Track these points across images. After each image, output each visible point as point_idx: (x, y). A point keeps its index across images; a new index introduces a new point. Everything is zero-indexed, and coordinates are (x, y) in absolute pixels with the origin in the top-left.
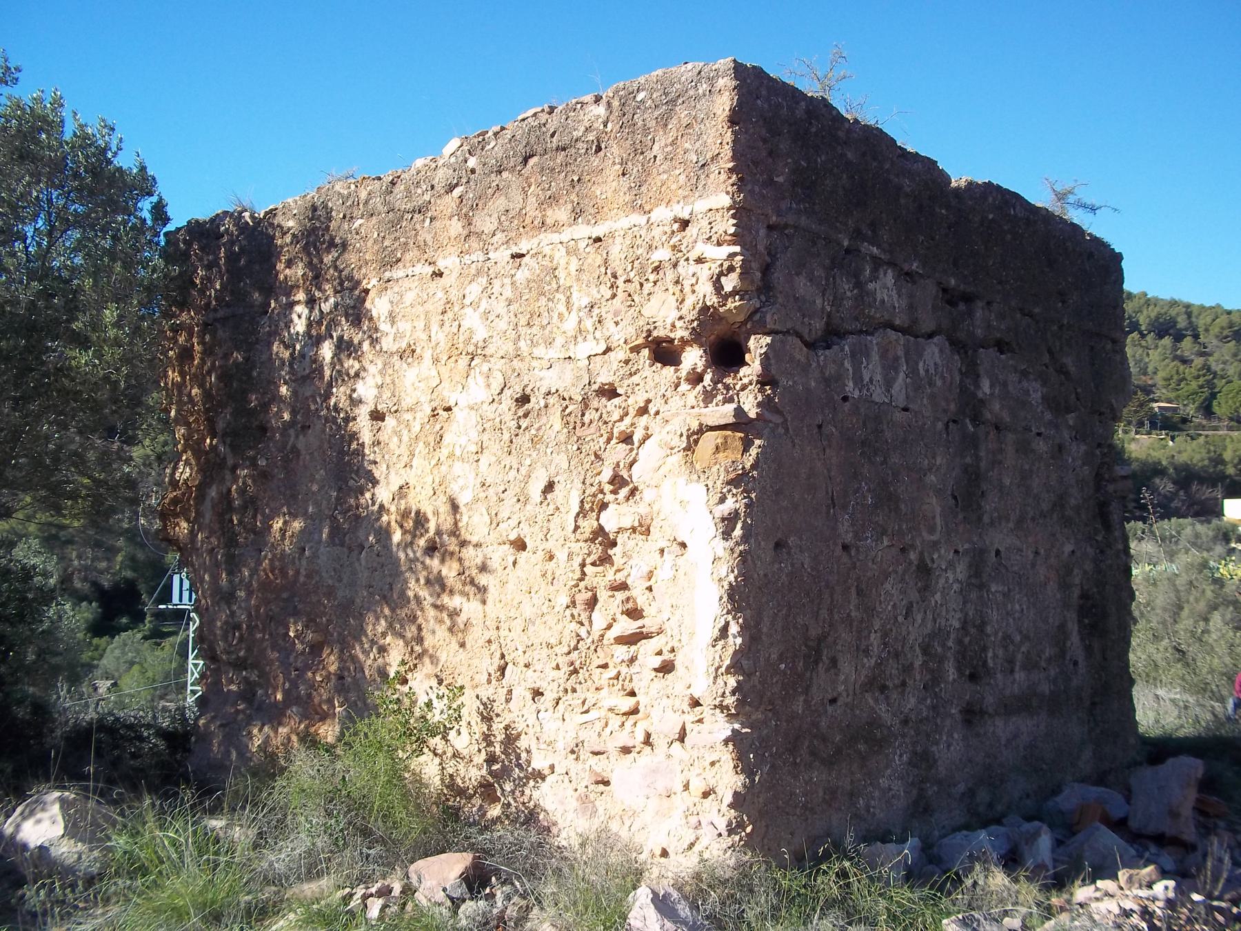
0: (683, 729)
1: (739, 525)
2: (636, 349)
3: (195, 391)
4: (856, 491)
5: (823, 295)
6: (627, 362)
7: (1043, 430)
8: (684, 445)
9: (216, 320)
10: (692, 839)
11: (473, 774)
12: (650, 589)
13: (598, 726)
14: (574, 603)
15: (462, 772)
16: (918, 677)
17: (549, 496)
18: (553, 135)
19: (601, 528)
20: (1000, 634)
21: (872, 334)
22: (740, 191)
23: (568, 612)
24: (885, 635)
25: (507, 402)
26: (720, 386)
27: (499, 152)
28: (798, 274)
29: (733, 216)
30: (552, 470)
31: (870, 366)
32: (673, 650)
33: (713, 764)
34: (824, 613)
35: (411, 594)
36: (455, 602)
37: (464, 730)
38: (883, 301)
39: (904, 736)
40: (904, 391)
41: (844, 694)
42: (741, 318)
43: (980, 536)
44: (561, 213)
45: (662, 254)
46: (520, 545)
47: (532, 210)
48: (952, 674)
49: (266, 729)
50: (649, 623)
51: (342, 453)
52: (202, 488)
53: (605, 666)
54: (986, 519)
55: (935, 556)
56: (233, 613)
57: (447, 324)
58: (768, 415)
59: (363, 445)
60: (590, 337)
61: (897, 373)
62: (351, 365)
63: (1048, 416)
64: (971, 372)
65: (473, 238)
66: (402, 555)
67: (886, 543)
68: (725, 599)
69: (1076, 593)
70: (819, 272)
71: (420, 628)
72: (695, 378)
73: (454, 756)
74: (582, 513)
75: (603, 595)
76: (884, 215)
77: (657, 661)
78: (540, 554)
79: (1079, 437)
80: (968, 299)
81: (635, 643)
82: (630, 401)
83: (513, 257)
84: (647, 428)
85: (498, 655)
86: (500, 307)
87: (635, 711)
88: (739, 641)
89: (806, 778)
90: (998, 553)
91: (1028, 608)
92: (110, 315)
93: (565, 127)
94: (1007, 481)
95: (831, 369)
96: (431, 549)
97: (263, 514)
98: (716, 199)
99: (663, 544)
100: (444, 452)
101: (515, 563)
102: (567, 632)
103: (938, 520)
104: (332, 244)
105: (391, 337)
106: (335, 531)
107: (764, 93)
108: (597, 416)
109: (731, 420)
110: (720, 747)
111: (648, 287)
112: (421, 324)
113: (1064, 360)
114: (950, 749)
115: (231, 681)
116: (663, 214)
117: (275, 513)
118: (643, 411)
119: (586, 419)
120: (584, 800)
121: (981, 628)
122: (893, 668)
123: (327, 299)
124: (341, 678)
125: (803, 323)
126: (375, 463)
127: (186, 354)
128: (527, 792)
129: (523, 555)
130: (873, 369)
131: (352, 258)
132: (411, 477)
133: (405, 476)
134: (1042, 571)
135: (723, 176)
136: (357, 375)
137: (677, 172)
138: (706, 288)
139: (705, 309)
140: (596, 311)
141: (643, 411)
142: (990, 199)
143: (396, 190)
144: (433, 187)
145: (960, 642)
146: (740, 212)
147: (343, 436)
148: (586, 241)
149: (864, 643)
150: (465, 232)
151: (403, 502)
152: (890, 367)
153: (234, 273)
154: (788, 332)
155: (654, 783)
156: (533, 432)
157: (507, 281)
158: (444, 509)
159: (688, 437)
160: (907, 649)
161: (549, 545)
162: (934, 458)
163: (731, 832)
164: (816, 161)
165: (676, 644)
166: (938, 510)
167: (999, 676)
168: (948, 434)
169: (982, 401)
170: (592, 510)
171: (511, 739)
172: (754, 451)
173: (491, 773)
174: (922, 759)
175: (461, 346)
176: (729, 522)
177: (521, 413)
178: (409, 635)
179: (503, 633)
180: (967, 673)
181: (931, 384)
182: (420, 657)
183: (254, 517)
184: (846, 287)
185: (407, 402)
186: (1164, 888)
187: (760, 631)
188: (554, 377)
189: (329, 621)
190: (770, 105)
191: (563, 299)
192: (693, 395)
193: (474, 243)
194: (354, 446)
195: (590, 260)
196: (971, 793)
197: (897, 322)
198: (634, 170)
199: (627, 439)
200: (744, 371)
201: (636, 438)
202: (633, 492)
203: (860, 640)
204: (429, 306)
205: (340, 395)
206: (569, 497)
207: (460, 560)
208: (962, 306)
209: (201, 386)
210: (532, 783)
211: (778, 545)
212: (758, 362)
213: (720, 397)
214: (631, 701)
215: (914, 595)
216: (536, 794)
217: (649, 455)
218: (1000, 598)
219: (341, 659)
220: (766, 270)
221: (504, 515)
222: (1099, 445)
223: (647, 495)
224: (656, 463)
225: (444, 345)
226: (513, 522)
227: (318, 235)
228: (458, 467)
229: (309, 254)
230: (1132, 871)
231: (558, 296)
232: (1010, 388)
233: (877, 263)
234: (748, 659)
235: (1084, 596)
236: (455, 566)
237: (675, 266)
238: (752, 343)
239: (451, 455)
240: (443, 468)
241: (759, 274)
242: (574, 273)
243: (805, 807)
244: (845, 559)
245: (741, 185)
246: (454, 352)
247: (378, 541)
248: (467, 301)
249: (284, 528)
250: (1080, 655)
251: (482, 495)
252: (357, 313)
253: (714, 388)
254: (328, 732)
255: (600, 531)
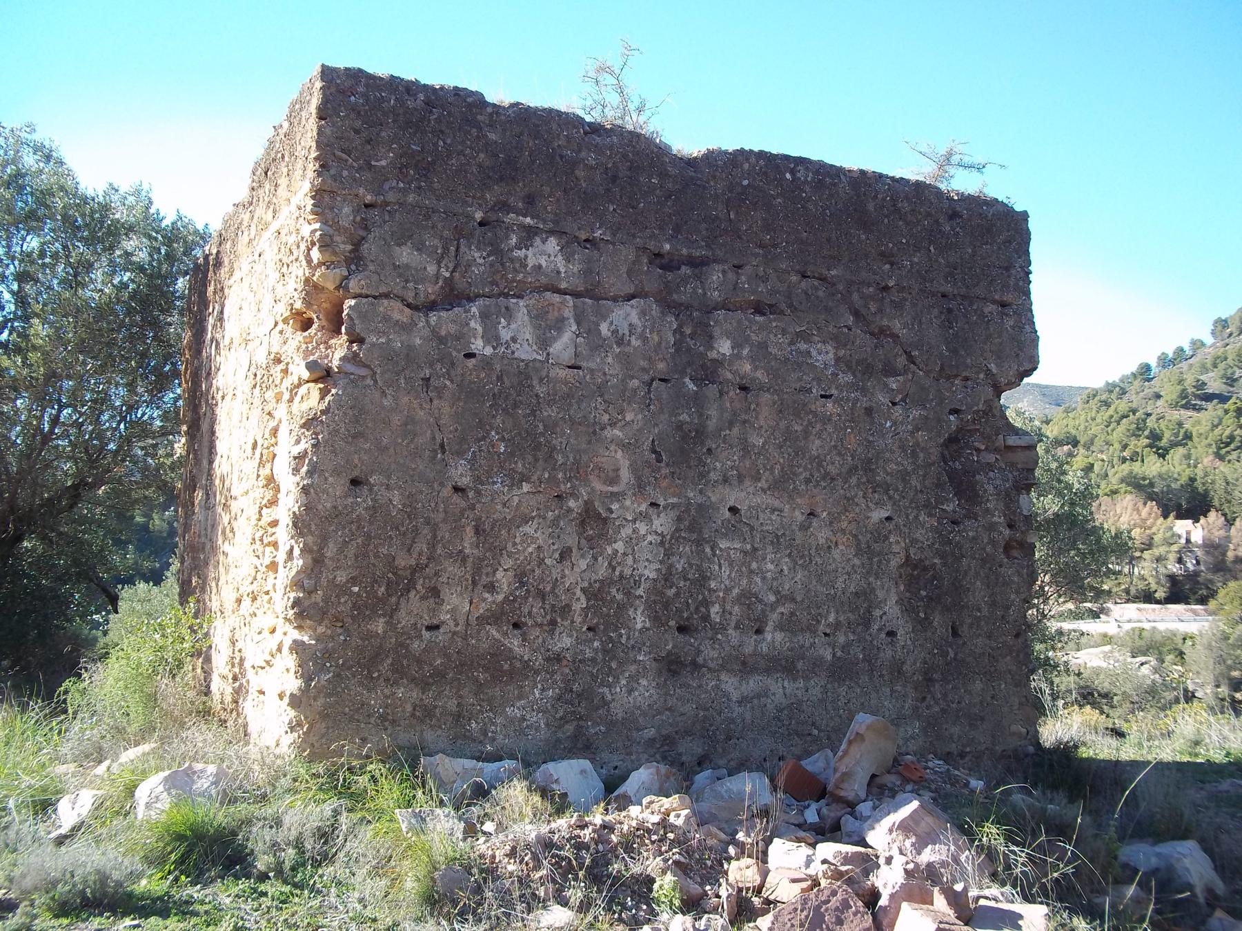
54: (713, 476)
88: (301, 562)
163: (292, 729)
176: (300, 458)
211: (355, 482)
234: (310, 578)
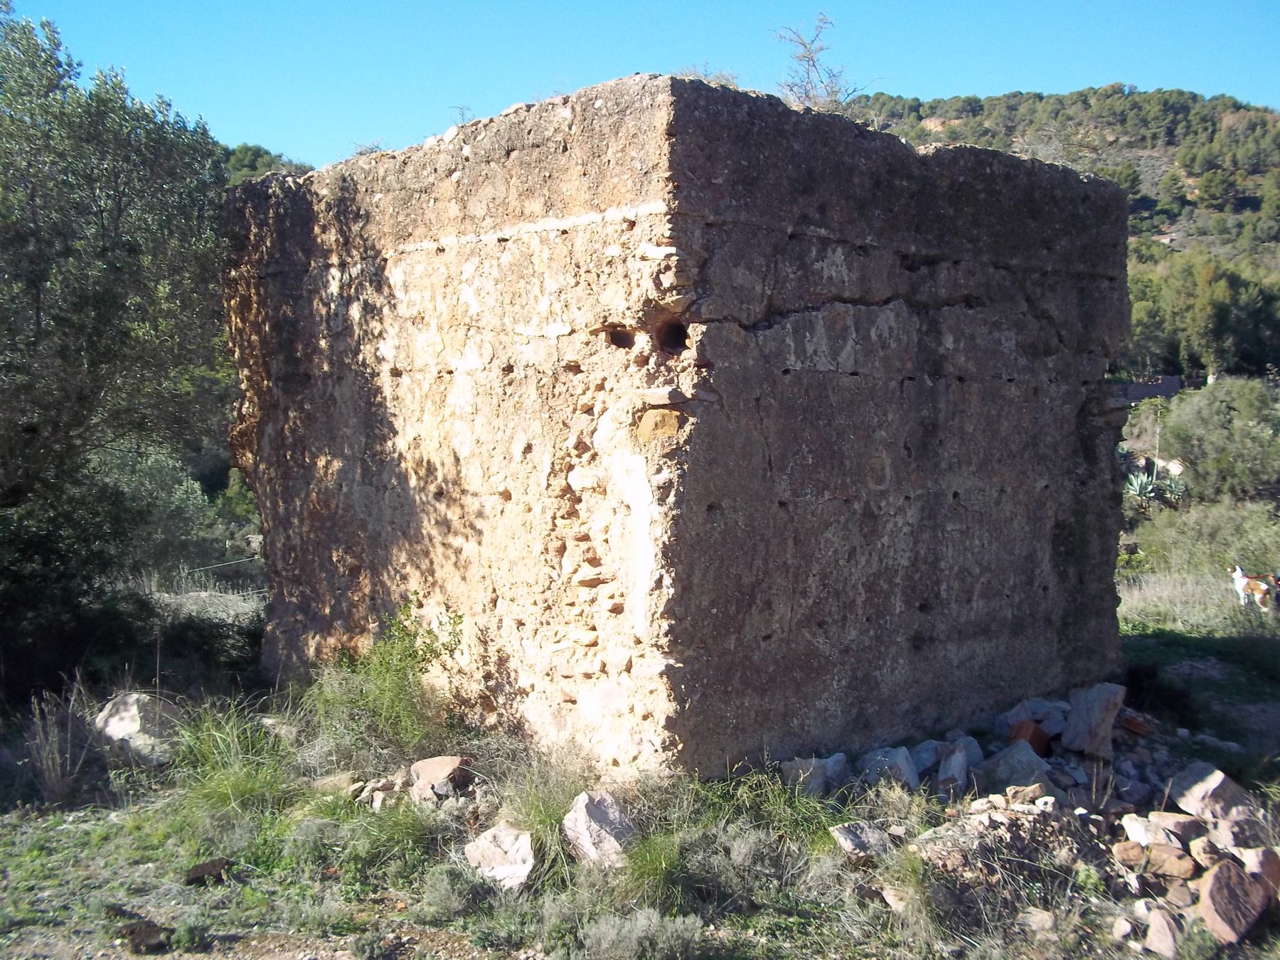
0: (630, 661)
1: (673, 493)
2: (595, 333)
3: (254, 337)
4: (797, 453)
5: (764, 280)
6: (587, 344)
7: (1016, 375)
8: (630, 421)
9: (268, 275)
10: (636, 753)
11: (474, 688)
12: (606, 541)
13: (568, 654)
14: (547, 549)
15: (465, 686)
16: (860, 612)
17: (528, 456)
18: (529, 133)
19: (569, 486)
20: (956, 568)
21: (818, 309)
22: (675, 198)
23: (543, 558)
24: (824, 577)
25: (496, 372)
26: (662, 368)
27: (487, 144)
28: (735, 266)
29: (669, 221)
30: (530, 435)
31: (815, 339)
32: (622, 595)
33: (651, 692)
34: (759, 562)
35: (424, 532)
36: (456, 541)
37: (466, 651)
38: (830, 278)
39: (843, 664)
40: (852, 358)
41: (779, 631)
42: (679, 310)
43: (936, 481)
44: (535, 206)
45: (614, 251)
46: (507, 496)
47: (513, 202)
48: (898, 606)
49: (318, 637)
50: (605, 571)
51: (370, 404)
52: (261, 424)
53: (572, 604)
54: (944, 465)
55: (883, 504)
56: (288, 538)
57: (448, 297)
58: (703, 395)
59: (385, 398)
60: (559, 319)
61: (845, 340)
62: (375, 326)
63: (1023, 361)
64: (934, 329)
65: (467, 221)
66: (417, 498)
67: (827, 497)
68: (660, 555)
69: (1049, 524)
70: (759, 261)
71: (432, 563)
72: (642, 361)
73: (459, 671)
74: (553, 472)
75: (570, 544)
76: (834, 197)
77: (610, 604)
78: (522, 506)
79: (1062, 375)
80: (931, 262)
81: (595, 586)
82: (591, 377)
83: (499, 241)
84: (604, 402)
85: (490, 589)
86: (489, 285)
87: (595, 644)
88: (672, 591)
89: (738, 703)
90: (956, 495)
91: (990, 543)
92: (163, 289)
93: (538, 126)
94: (970, 429)
95: (772, 346)
96: (440, 494)
97: (310, 451)
98: (654, 206)
99: (616, 505)
100: (447, 411)
101: (502, 512)
102: (541, 575)
103: (888, 469)
104: (357, 216)
105: (405, 304)
106: (366, 470)
107: (702, 103)
108: (564, 389)
109: (667, 402)
110: (657, 678)
111: (603, 278)
112: (428, 295)
113: (1045, 306)
114: (896, 672)
115: (291, 595)
116: (615, 215)
117: (320, 451)
118: (601, 387)
119: (557, 391)
120: (558, 714)
121: (934, 565)
122: (833, 606)
123: (355, 264)
124: (372, 599)
125: (741, 309)
126: (395, 415)
127: (245, 304)
128: (515, 705)
129: (509, 506)
130: (818, 341)
131: (372, 229)
132: (422, 430)
133: (423, 429)
134: (1008, 508)
135: (662, 184)
136: (380, 334)
137: (626, 177)
138: (648, 284)
139: (648, 302)
140: (563, 296)
141: (601, 387)
142: (962, 163)
143: (407, 170)
144: (436, 170)
145: (908, 578)
146: (675, 217)
147: (370, 389)
148: (556, 233)
149: (801, 586)
150: (461, 215)
151: (417, 452)
152: (837, 337)
153: (282, 236)
154: (725, 318)
155: (606, 706)
156: (516, 398)
157: (495, 262)
158: (449, 461)
159: (634, 414)
160: (848, 589)
161: (528, 499)
162: (885, 414)
163: (665, 749)
164: (758, 158)
165: (625, 591)
166: (888, 462)
167: (953, 605)
168: (902, 392)
169: (944, 357)
170: (561, 470)
171: (502, 661)
172: (688, 428)
173: (487, 687)
174: (862, 684)
175: (459, 317)
176: (665, 489)
177: (506, 382)
178: (424, 567)
179: (494, 571)
180: (917, 604)
181: (884, 346)
182: (434, 584)
183: (303, 454)
184: (790, 270)
185: (418, 364)
186: (1046, 803)
187: (691, 582)
188: (533, 353)
189: (363, 550)
190: (708, 115)
191: (538, 283)
192: (638, 375)
193: (468, 225)
194: (379, 399)
195: (558, 251)
196: (916, 709)
197: (847, 295)
198: (593, 171)
199: (589, 410)
200: (685, 354)
201: (596, 410)
202: (594, 457)
203: (797, 583)
204: (434, 279)
205: (367, 351)
206: (543, 457)
207: (462, 507)
208: (924, 270)
209: (258, 333)
210: (519, 698)
211: (711, 508)
212: (694, 348)
213: (661, 379)
214: (592, 635)
215: (857, 540)
216: (521, 708)
217: (606, 425)
218: (957, 536)
219: (374, 585)
220: (703, 265)
221: (494, 469)
222: (1085, 383)
223: (603, 459)
224: (610, 433)
225: (446, 317)
226: (501, 476)
227: (347, 207)
228: (459, 426)
229: (340, 221)
230: (1018, 788)
231: (535, 280)
232: (978, 341)
233: (824, 243)
235: (1058, 525)
236: (458, 511)
237: (624, 261)
238: (690, 331)
239: (453, 414)
240: (447, 425)
241: (695, 271)
242: (546, 260)
243: (736, 727)
244: (782, 514)
245: (677, 192)
246: (454, 322)
247: (399, 483)
248: (464, 278)
249: (328, 465)
250: (1052, 581)
251: (477, 451)
252: (378, 279)
253: (658, 371)
254: (364, 644)
255: (568, 489)
